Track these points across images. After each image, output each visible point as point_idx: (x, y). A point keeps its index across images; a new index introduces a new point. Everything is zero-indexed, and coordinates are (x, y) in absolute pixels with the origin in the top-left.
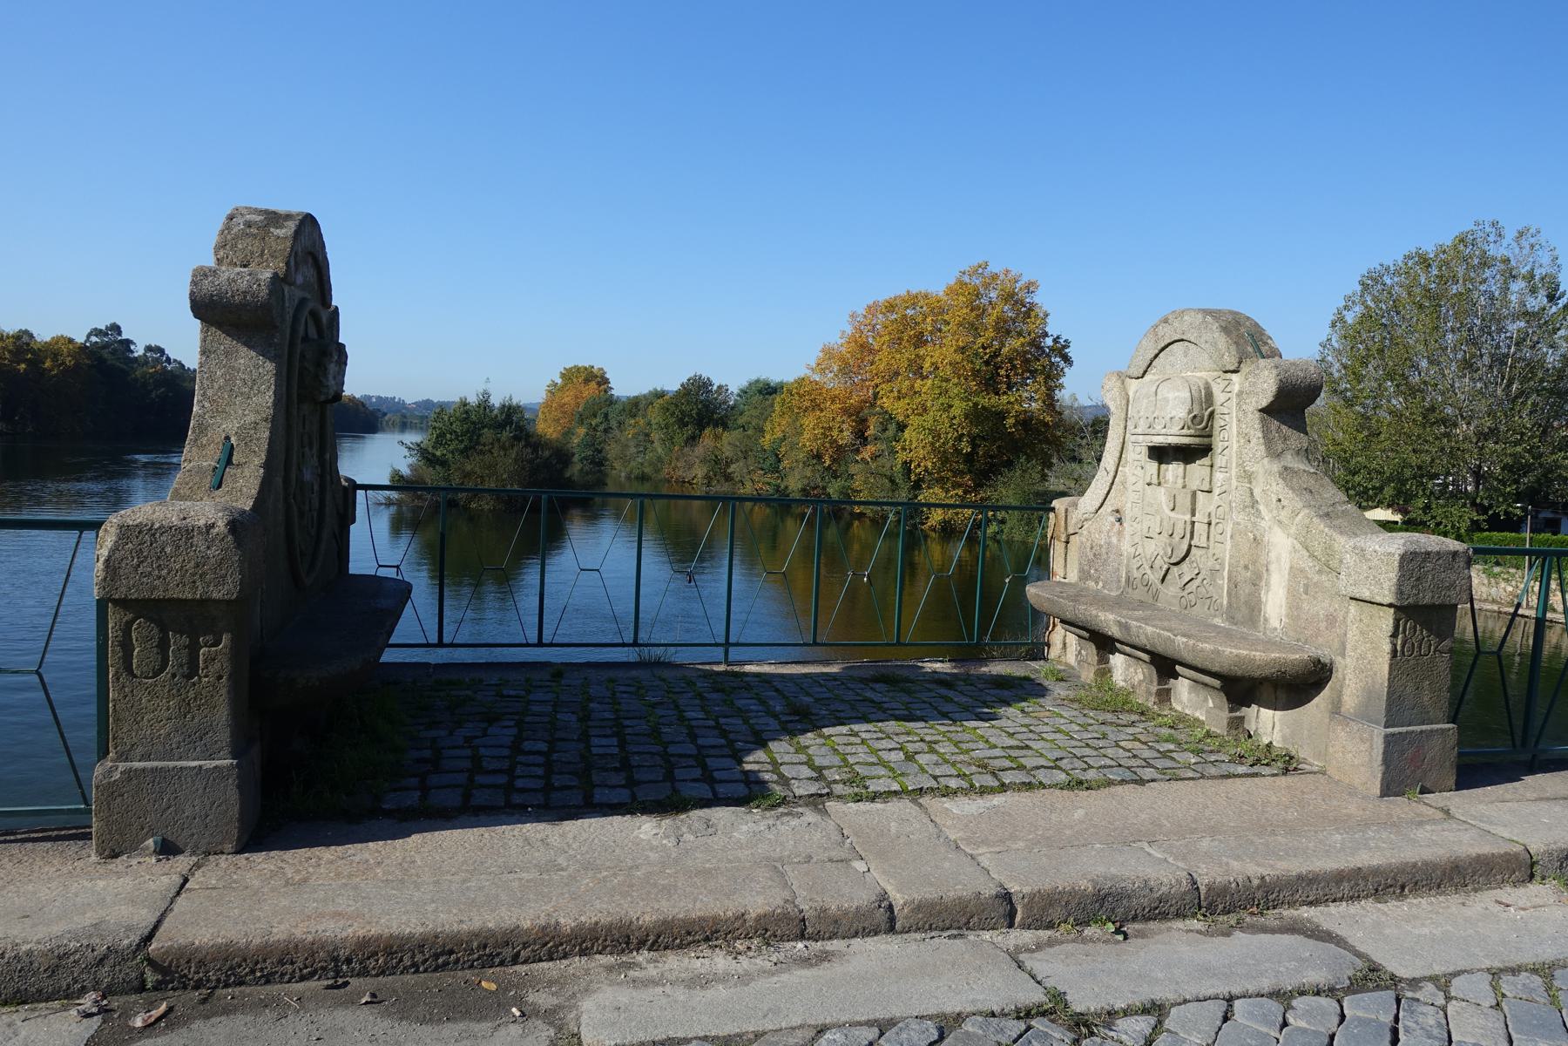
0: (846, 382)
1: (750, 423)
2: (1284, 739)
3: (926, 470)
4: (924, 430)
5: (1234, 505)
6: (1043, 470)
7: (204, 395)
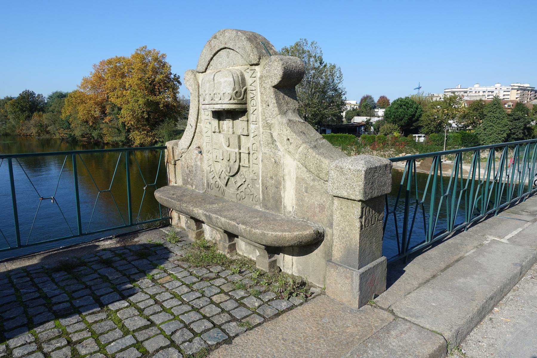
0: (95, 92)
1: (54, 110)
2: (299, 271)
3: (131, 125)
4: (129, 110)
5: (262, 143)
6: (175, 122)
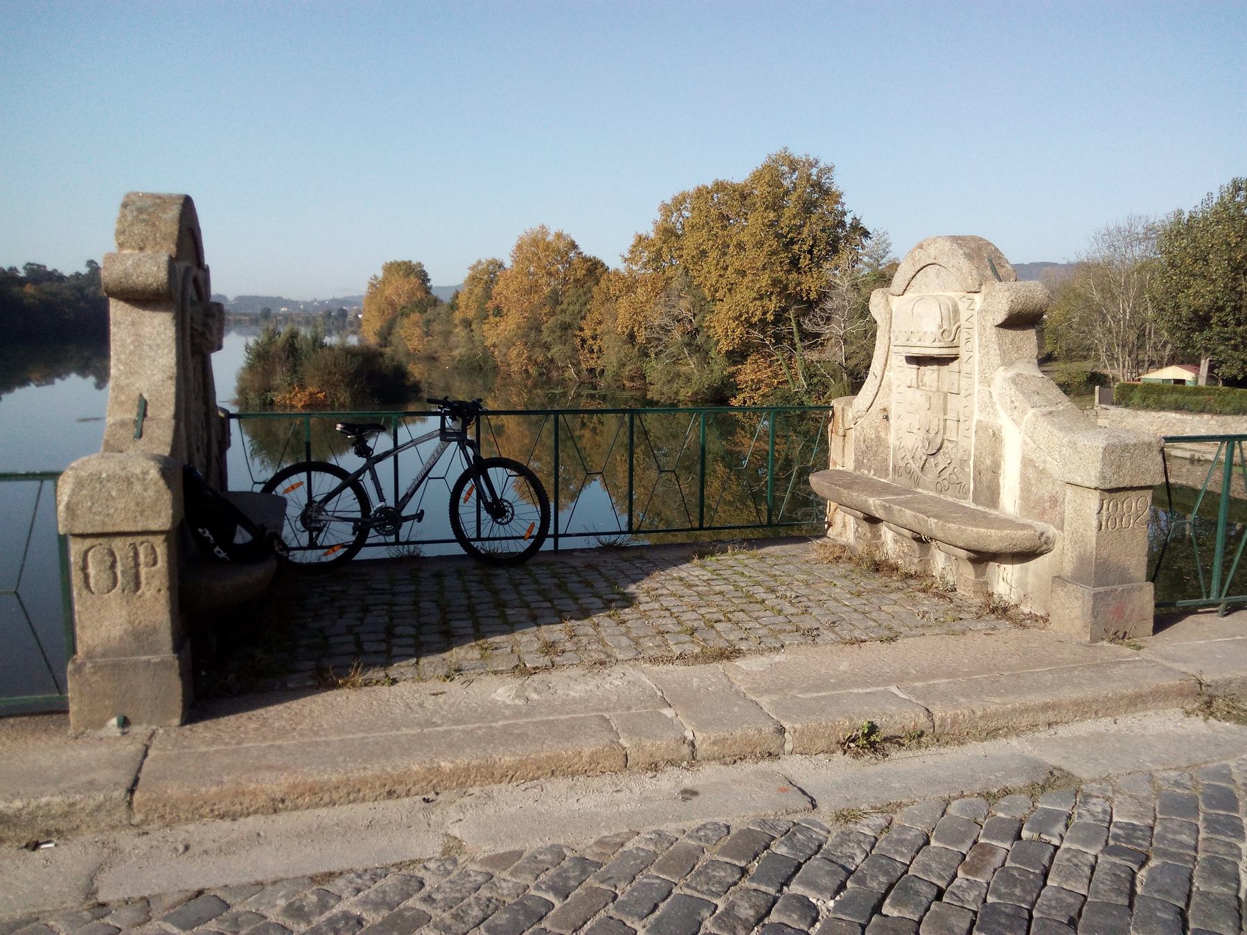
7: (118, 360)
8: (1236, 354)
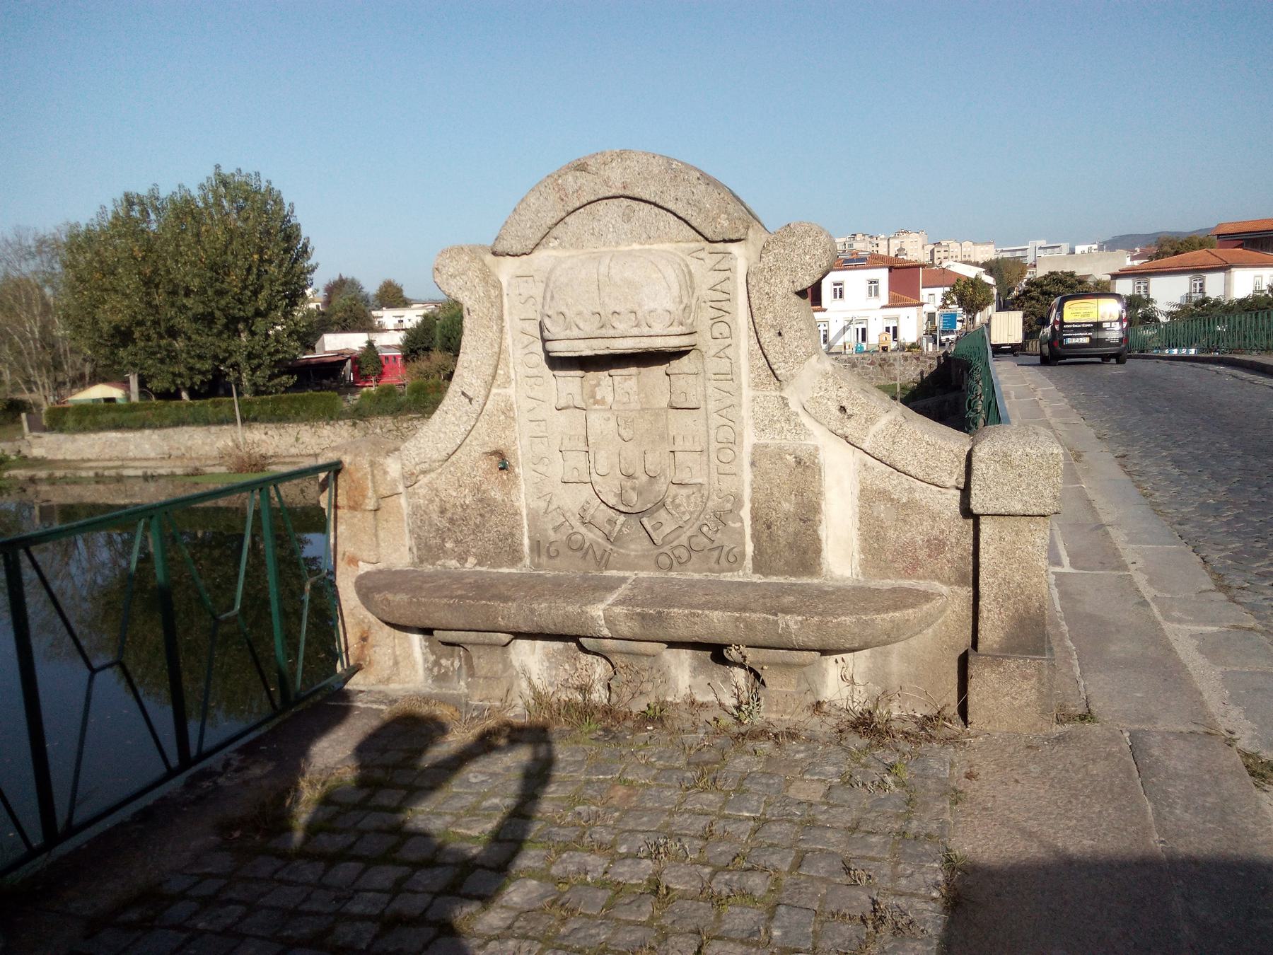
8: (165, 368)
